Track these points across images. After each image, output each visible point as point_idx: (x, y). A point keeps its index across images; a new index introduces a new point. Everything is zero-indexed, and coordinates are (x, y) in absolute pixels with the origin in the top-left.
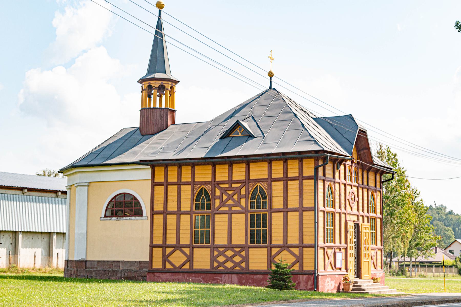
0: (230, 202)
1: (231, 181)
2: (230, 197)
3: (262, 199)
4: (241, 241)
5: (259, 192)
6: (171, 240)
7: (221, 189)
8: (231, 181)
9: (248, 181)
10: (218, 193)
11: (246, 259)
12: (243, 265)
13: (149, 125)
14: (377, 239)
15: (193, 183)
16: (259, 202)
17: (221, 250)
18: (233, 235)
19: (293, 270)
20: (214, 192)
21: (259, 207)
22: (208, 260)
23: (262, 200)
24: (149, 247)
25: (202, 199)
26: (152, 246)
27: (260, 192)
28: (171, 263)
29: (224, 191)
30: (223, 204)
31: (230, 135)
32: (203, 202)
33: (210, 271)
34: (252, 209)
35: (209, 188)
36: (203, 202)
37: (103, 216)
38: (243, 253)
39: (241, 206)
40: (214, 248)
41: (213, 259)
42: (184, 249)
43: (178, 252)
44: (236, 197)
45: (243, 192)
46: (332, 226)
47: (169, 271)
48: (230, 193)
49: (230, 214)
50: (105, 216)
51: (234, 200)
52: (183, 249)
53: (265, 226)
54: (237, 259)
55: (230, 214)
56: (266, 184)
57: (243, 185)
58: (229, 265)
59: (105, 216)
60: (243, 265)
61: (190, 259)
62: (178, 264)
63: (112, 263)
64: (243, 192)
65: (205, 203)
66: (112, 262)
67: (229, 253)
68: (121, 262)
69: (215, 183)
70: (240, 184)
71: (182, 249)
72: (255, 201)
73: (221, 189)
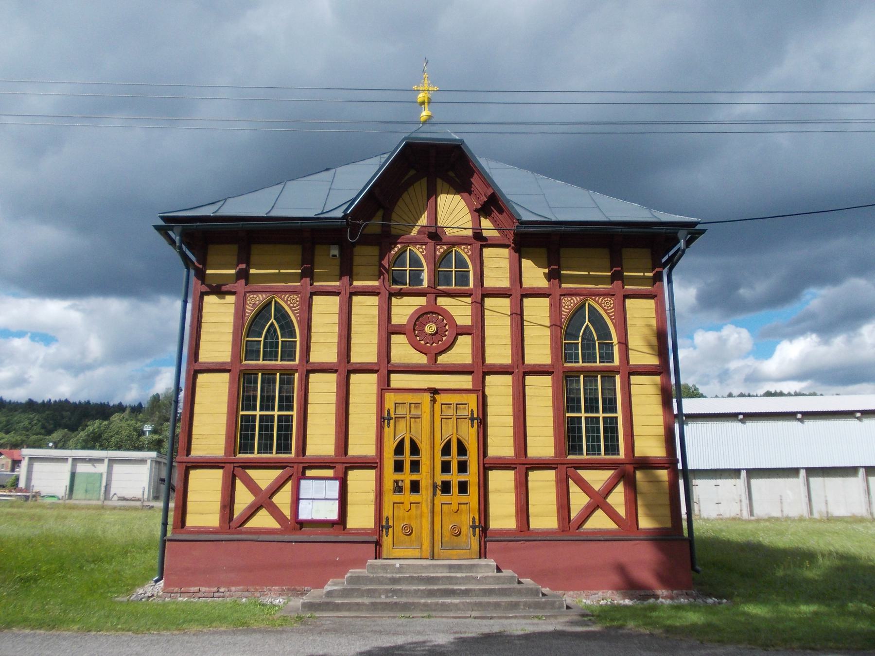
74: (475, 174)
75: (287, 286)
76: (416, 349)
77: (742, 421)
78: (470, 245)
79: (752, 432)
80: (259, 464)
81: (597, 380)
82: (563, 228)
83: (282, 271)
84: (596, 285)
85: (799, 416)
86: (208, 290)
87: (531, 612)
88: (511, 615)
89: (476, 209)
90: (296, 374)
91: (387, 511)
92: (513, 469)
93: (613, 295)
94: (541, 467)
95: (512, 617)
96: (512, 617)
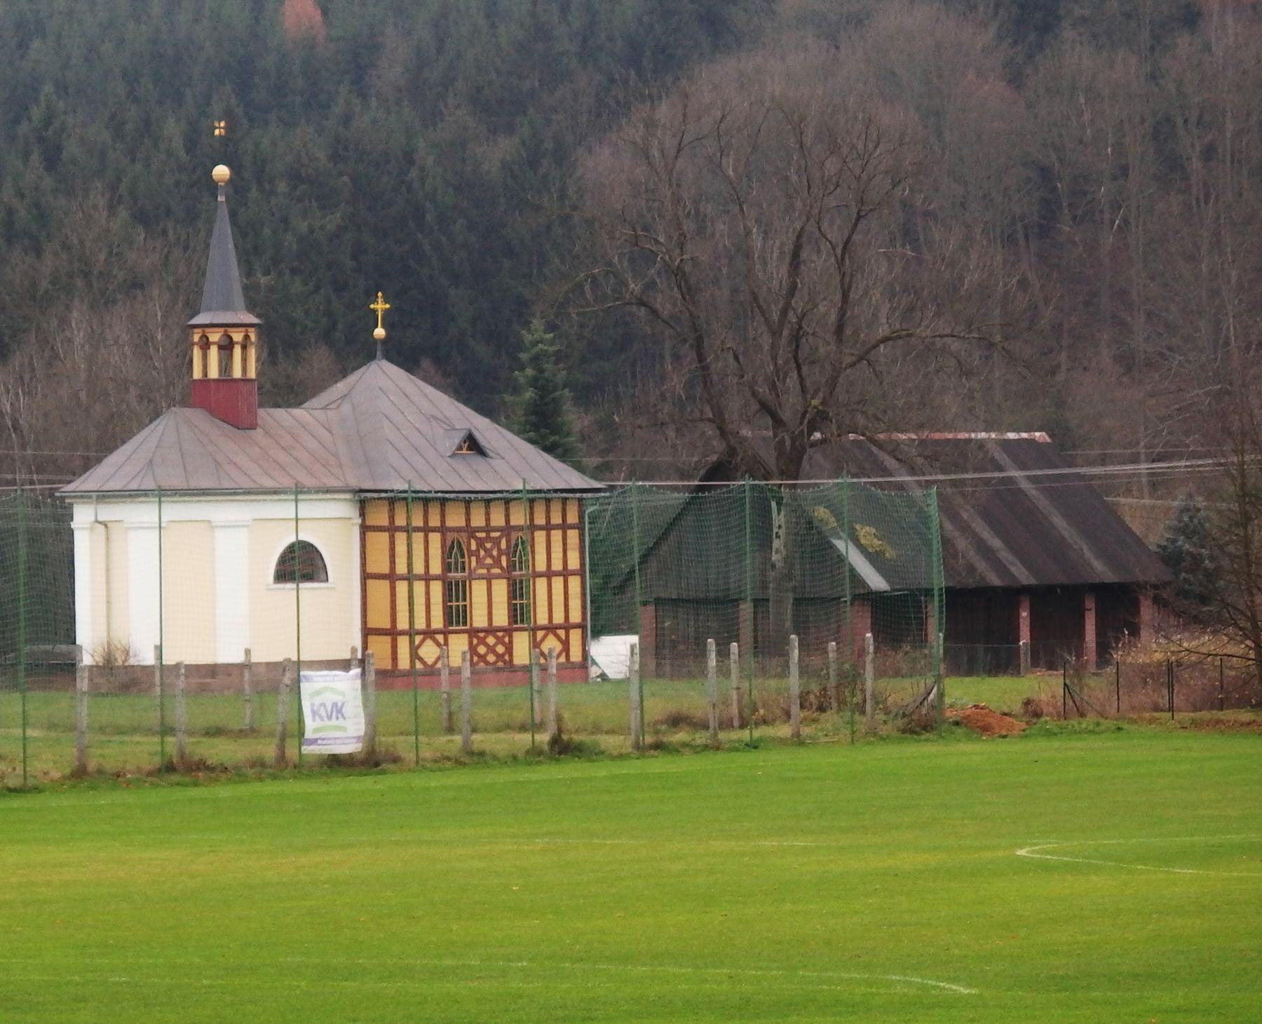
1: (488, 529)
6: (420, 624)
8: (488, 529)
9: (507, 529)
10: (474, 547)
14: (538, 610)
15: (443, 529)
17: (482, 635)
20: (469, 544)
24: (174, 663)
29: (481, 543)
35: (463, 537)
39: (502, 568)
40: (473, 633)
46: (451, 607)
49: (489, 579)
51: (485, 558)
53: (465, 600)
55: (489, 579)
62: (430, 661)
64: (503, 545)
69: (470, 531)
71: (888, 581)
73: (500, 538)
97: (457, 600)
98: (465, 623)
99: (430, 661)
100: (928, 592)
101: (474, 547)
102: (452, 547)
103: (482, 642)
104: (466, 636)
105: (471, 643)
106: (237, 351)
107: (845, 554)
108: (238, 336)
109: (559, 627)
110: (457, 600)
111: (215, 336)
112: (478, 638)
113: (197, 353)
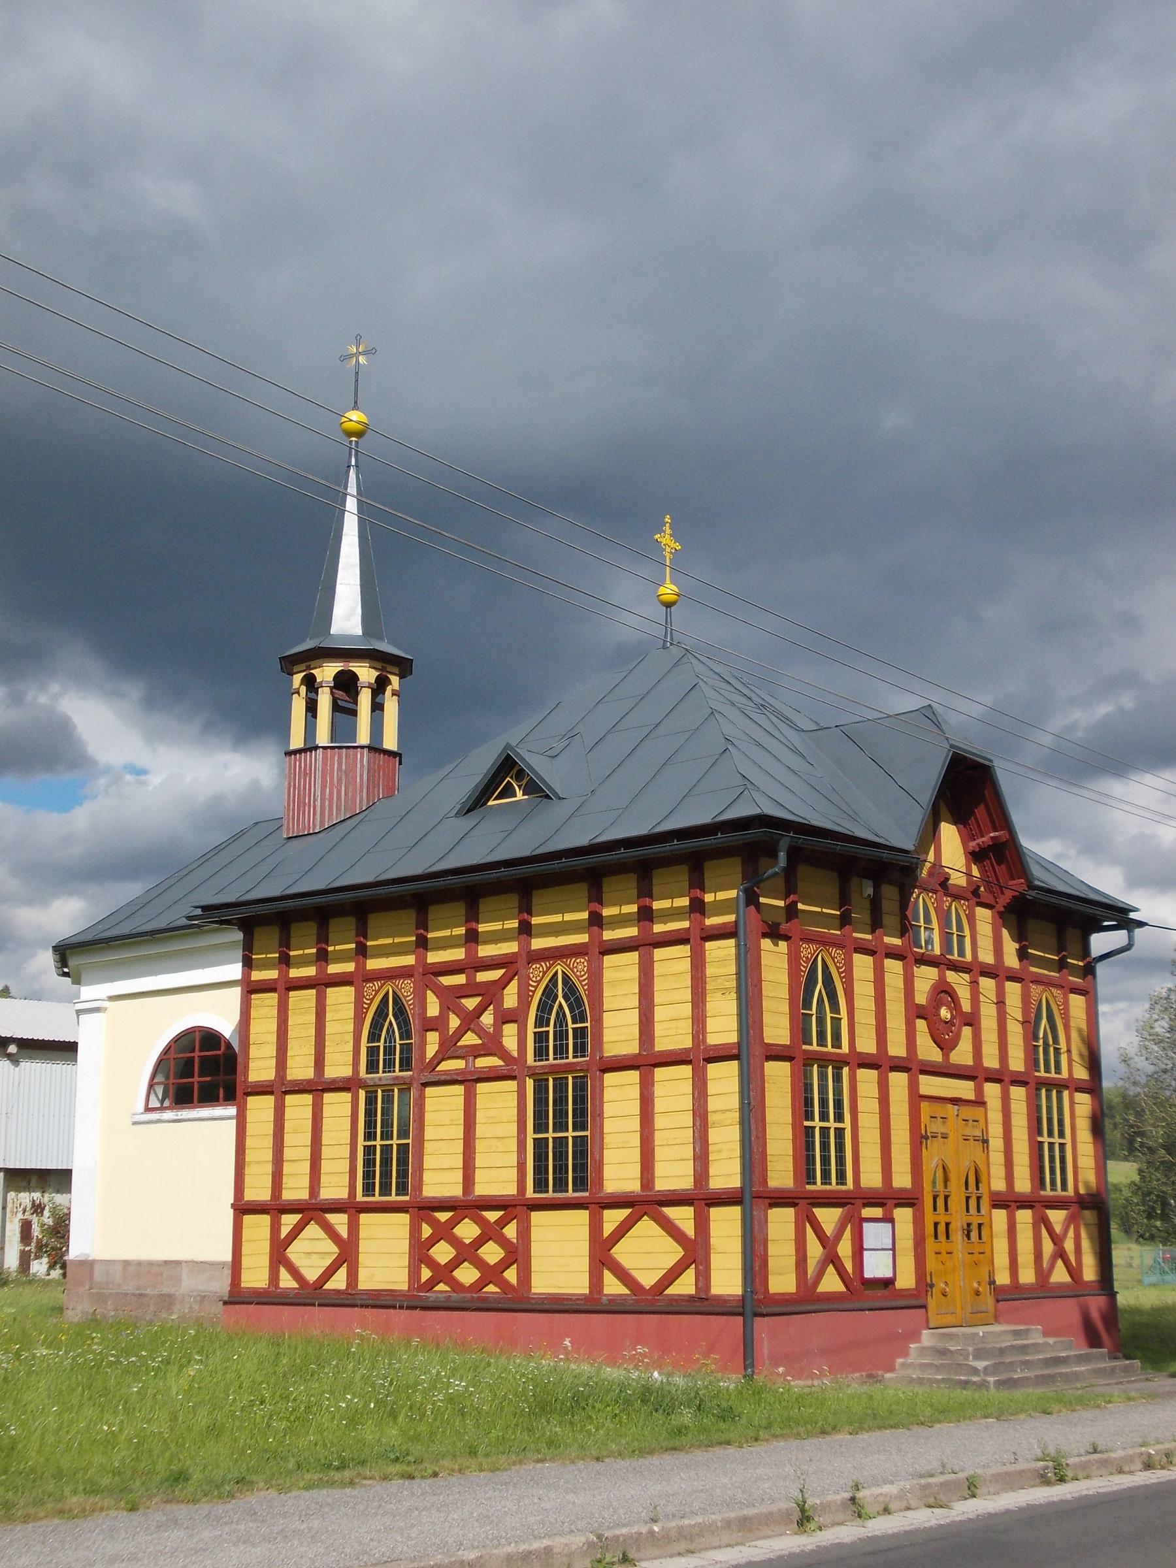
0: (470, 1039)
2: (470, 1020)
3: (573, 1023)
4: (334, 1188)
5: (393, 1015)
7: (441, 992)
10: (433, 1008)
11: (518, 1254)
12: (511, 1275)
13: (327, 796)
16: (561, 1031)
17: (443, 1216)
18: (636, 1154)
19: (1100, 1311)
21: (561, 1053)
22: (583, 1263)
23: (571, 1025)
24: (232, 1211)
25: (558, 1014)
26: (243, 1209)
27: (565, 997)
28: (623, 1275)
29: (451, 998)
30: (448, 1049)
31: (488, 800)
32: (390, 1042)
33: (607, 1307)
34: (539, 1060)
36: (390, 1042)
37: (141, 1108)
38: (511, 1231)
39: (503, 1054)
40: (423, 1209)
41: (419, 1252)
42: (671, 1212)
43: (646, 1226)
44: (487, 1019)
45: (510, 997)
47: (615, 1308)
48: (471, 1003)
50: (148, 1109)
52: (668, 1211)
54: (443, 1252)
56: (580, 965)
57: (511, 973)
58: (467, 1274)
59: (148, 1109)
60: (511, 1275)
61: (348, 1253)
63: (161, 1269)
65: (567, 1031)
66: (159, 1266)
67: (467, 1231)
68: (184, 1265)
70: (502, 971)
72: (547, 1029)
74: (982, 805)
75: (830, 934)
76: (935, 1042)
77: (14, 1060)
78: (968, 900)
79: (50, 1097)
80: (835, 1200)
81: (1040, 1095)
82: (1055, 900)
83: (824, 910)
84: (1049, 971)
85: (12, 1049)
86: (768, 931)
87: (1150, 1374)
88: (1133, 1379)
89: (973, 851)
90: (845, 1068)
91: (931, 1264)
92: (794, 1205)
93: (1063, 987)
94: (872, 1203)
95: (1135, 1381)
96: (1135, 1381)
97: (560, 1143)
98: (402, 1189)
99: (312, 1275)
100: (366, 937)
101: (433, 1008)
102: (381, 1013)
103: (444, 1233)
104: (404, 1218)
105: (415, 1231)
106: (365, 699)
107: (1005, 932)
108: (366, 673)
109: (336, 1207)
110: (560, 1143)
111: (327, 672)
112: (434, 1223)
113: (298, 706)
